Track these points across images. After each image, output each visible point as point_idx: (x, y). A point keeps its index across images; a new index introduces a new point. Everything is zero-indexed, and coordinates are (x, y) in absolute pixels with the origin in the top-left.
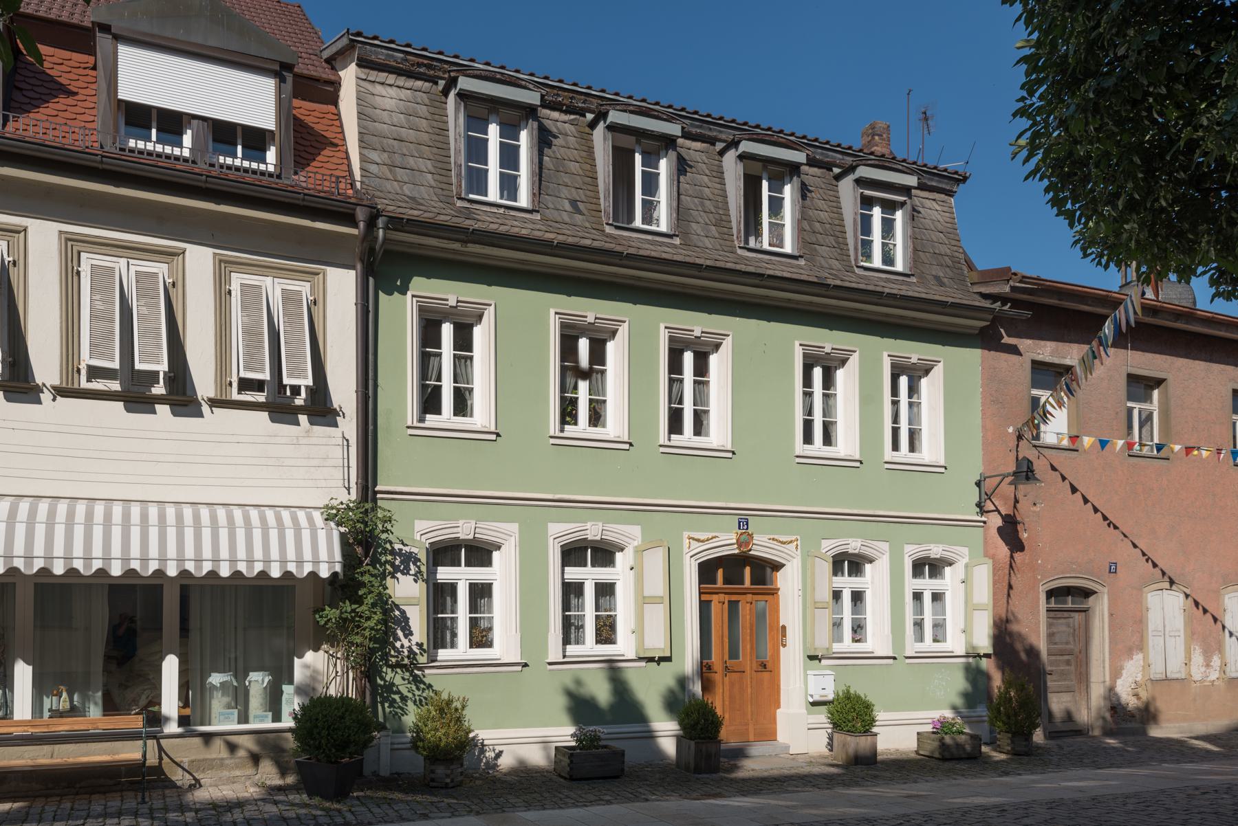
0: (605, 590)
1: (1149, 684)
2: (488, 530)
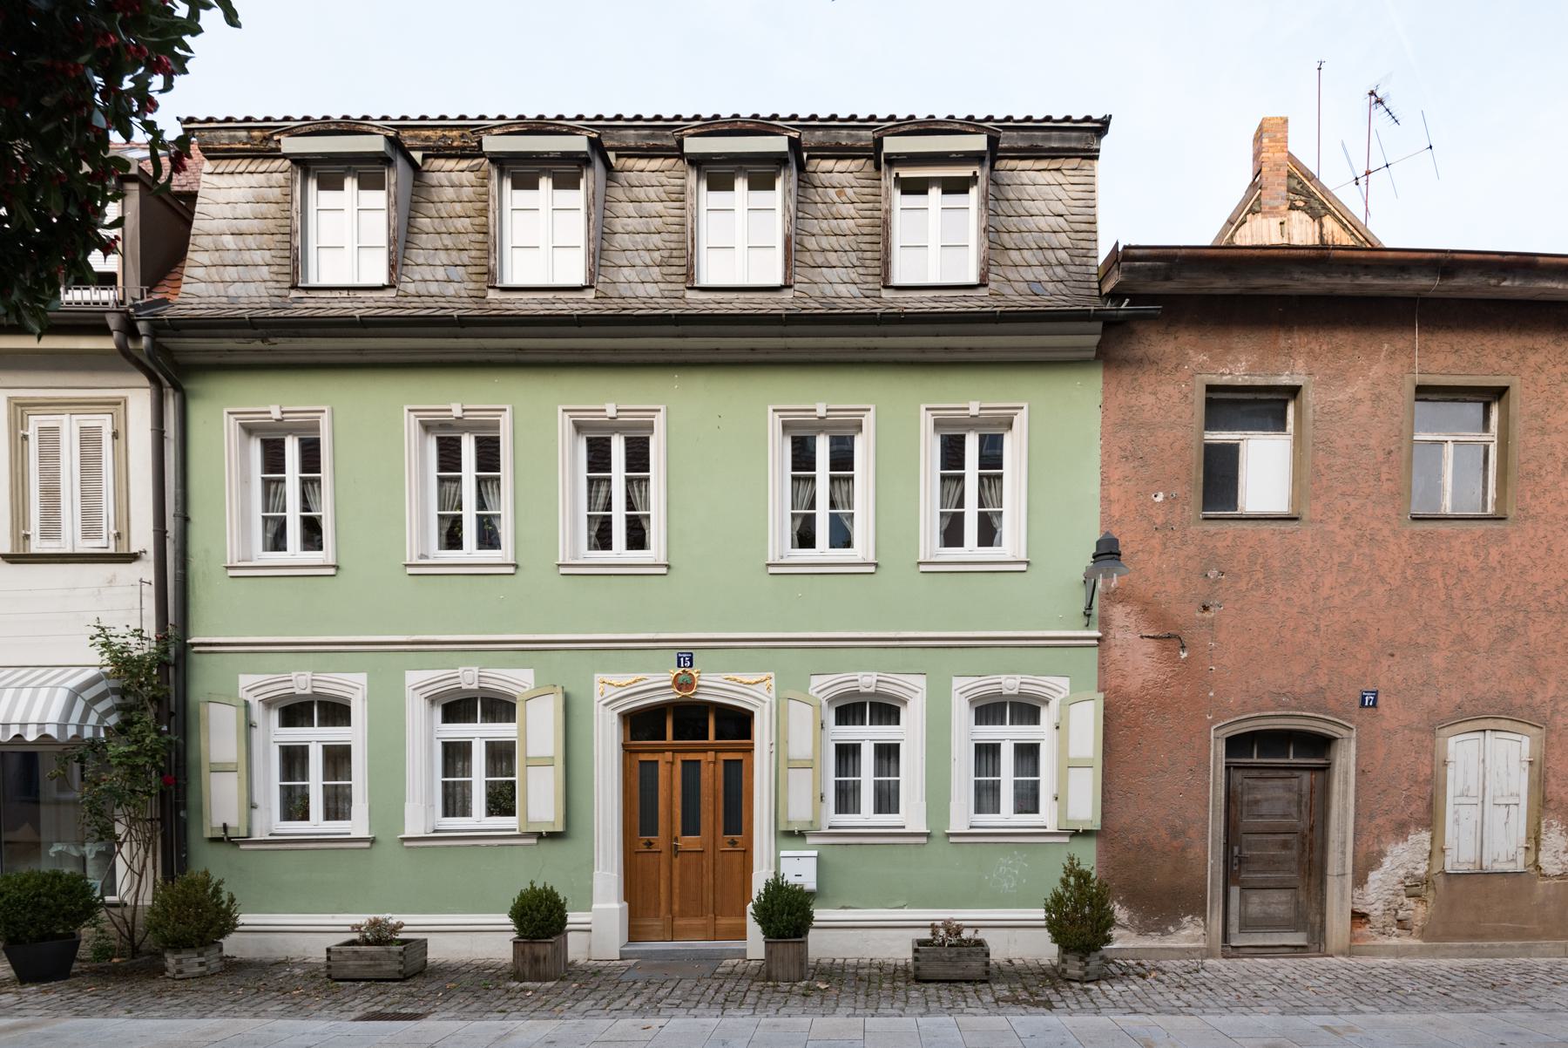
0: (888, 754)
1: (1441, 881)
2: (514, 679)
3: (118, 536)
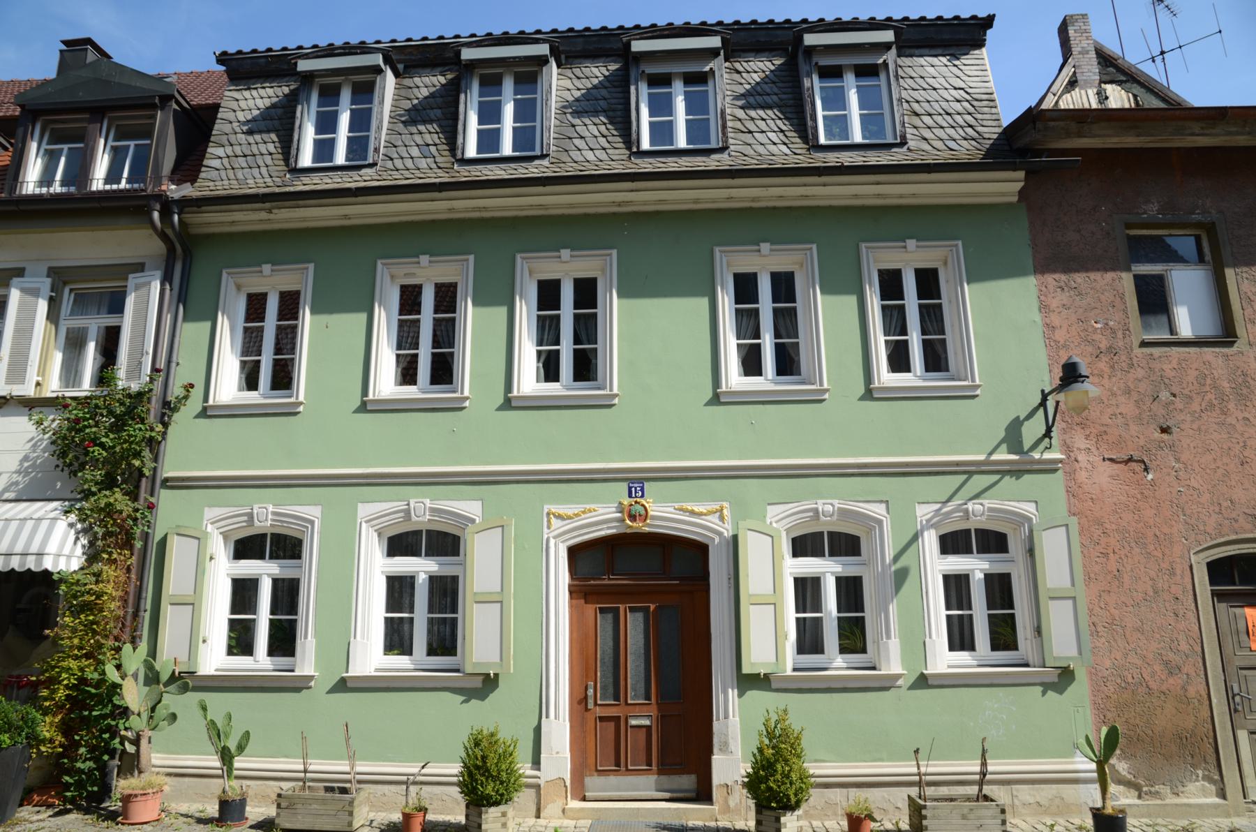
3: (38, 384)
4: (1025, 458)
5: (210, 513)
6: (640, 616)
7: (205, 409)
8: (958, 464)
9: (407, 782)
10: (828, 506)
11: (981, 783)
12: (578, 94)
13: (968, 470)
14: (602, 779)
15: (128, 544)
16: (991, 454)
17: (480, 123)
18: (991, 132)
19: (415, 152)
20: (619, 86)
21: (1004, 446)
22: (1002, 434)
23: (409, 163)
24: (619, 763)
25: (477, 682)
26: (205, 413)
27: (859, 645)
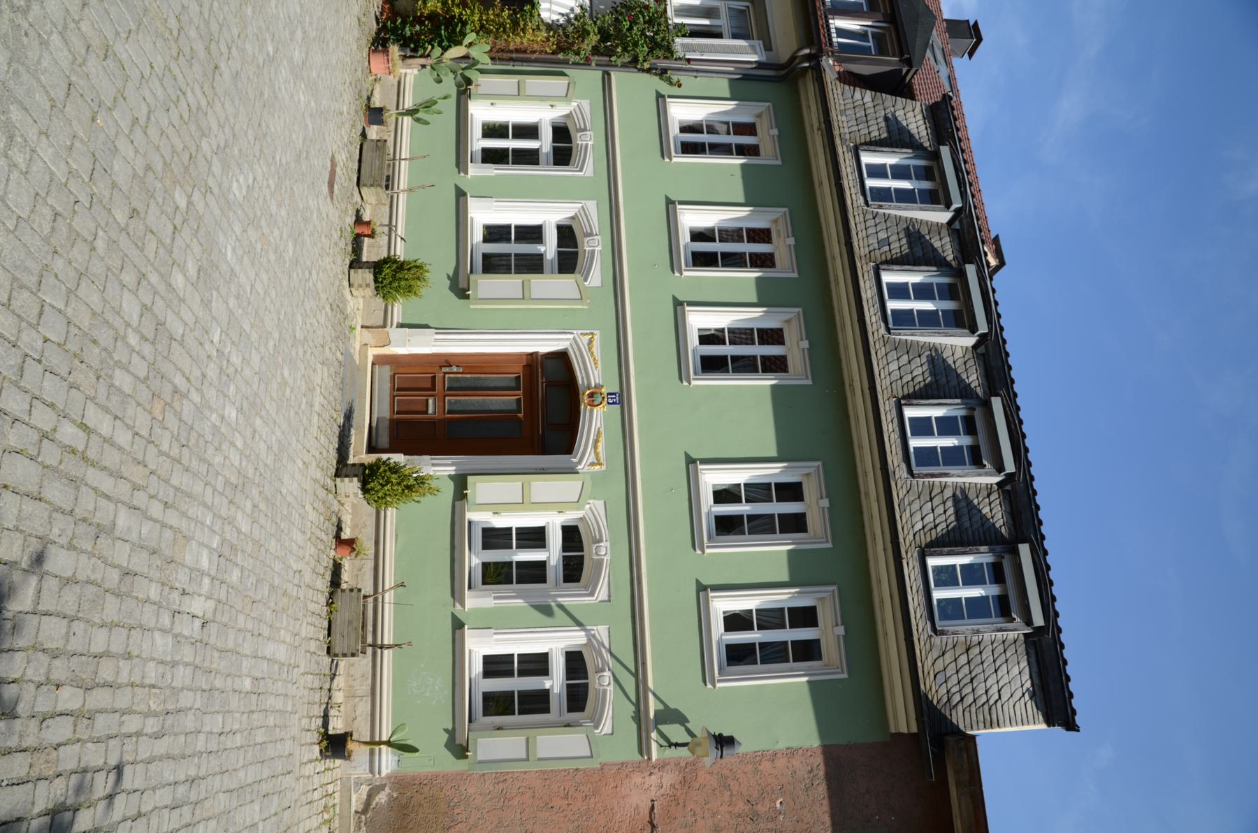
4: (652, 725)
5: (586, 104)
6: (514, 406)
7: (673, 203)
8: (644, 664)
9: (391, 227)
10: (605, 552)
11: (374, 645)
12: (950, 361)
13: (639, 673)
14: (388, 378)
15: (560, 49)
16: (654, 694)
17: (962, 566)
18: (959, 718)
19: (882, 235)
20: (962, 391)
21: (661, 707)
22: (672, 706)
23: (871, 231)
24: (400, 388)
25: (462, 285)
26: (660, 97)
27: (489, 580)
